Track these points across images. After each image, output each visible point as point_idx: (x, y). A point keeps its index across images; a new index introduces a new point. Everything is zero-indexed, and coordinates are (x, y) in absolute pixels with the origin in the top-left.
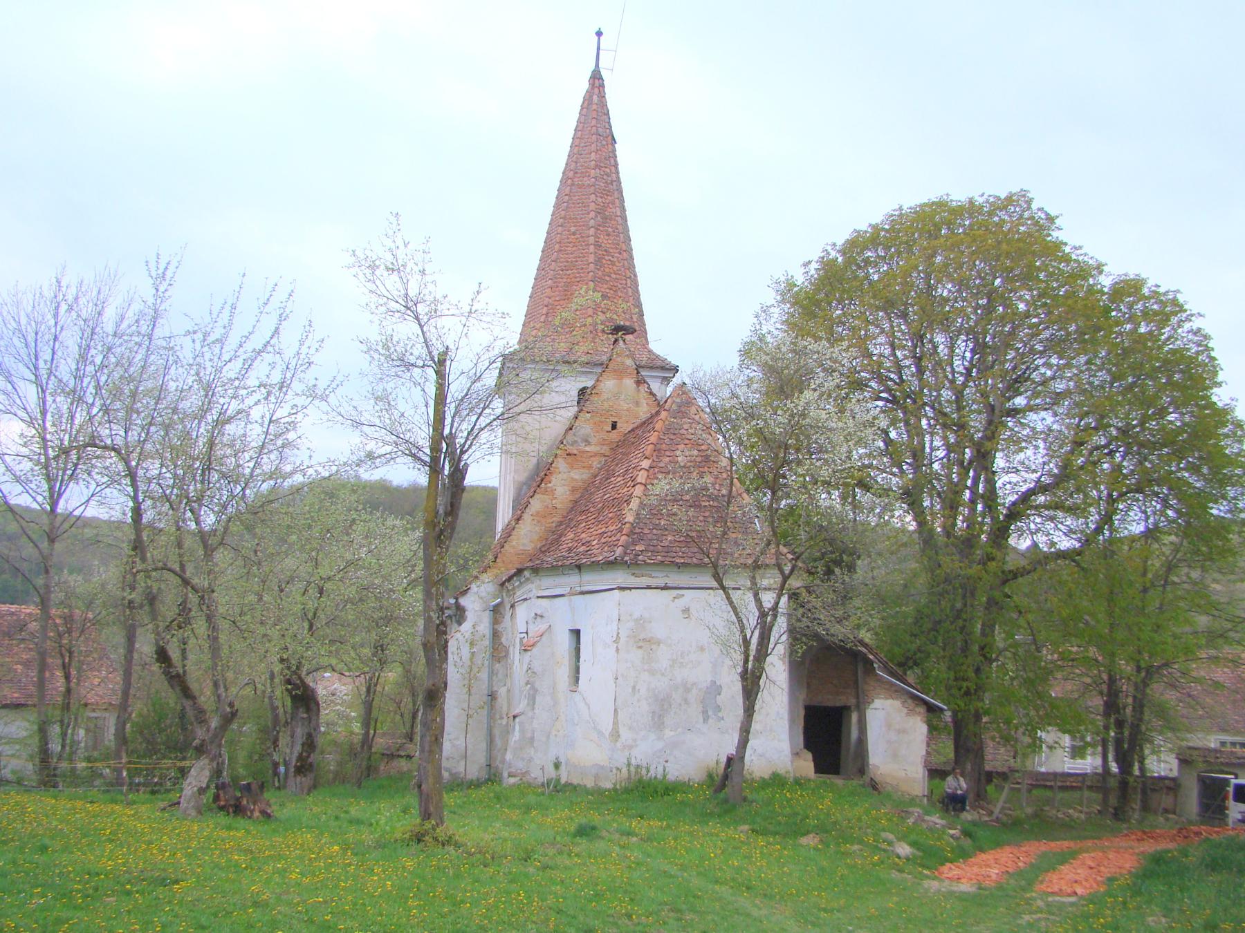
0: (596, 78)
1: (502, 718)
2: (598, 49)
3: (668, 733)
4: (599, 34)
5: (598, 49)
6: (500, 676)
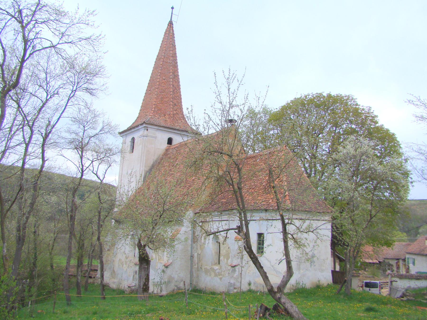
0: (171, 24)
1: (195, 265)
2: (172, 13)
3: (302, 271)
4: (173, 8)
5: (172, 13)
6: (195, 249)
